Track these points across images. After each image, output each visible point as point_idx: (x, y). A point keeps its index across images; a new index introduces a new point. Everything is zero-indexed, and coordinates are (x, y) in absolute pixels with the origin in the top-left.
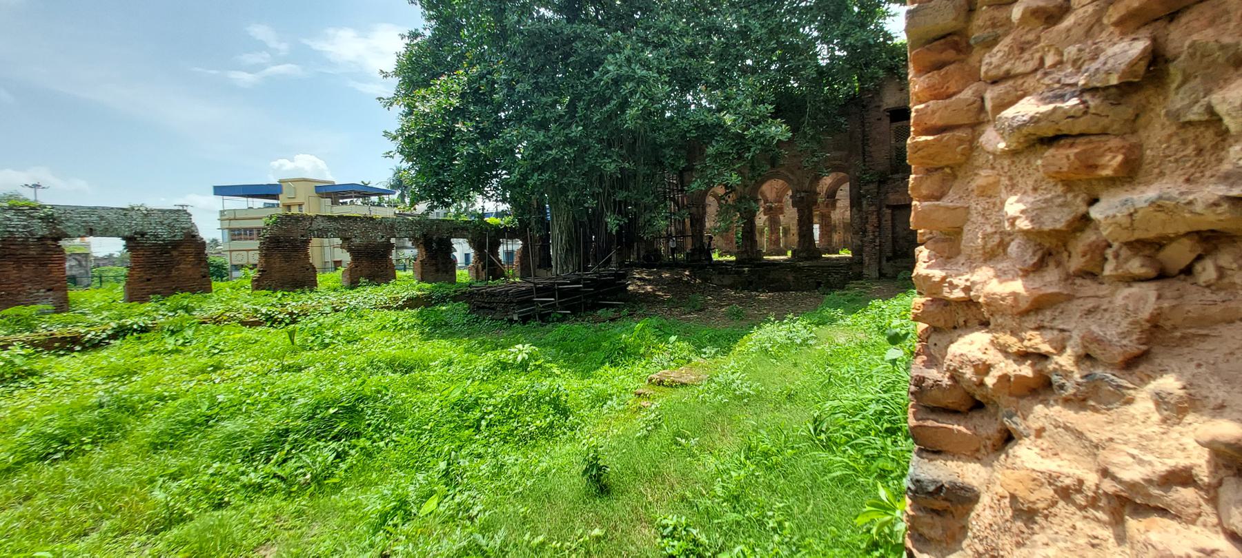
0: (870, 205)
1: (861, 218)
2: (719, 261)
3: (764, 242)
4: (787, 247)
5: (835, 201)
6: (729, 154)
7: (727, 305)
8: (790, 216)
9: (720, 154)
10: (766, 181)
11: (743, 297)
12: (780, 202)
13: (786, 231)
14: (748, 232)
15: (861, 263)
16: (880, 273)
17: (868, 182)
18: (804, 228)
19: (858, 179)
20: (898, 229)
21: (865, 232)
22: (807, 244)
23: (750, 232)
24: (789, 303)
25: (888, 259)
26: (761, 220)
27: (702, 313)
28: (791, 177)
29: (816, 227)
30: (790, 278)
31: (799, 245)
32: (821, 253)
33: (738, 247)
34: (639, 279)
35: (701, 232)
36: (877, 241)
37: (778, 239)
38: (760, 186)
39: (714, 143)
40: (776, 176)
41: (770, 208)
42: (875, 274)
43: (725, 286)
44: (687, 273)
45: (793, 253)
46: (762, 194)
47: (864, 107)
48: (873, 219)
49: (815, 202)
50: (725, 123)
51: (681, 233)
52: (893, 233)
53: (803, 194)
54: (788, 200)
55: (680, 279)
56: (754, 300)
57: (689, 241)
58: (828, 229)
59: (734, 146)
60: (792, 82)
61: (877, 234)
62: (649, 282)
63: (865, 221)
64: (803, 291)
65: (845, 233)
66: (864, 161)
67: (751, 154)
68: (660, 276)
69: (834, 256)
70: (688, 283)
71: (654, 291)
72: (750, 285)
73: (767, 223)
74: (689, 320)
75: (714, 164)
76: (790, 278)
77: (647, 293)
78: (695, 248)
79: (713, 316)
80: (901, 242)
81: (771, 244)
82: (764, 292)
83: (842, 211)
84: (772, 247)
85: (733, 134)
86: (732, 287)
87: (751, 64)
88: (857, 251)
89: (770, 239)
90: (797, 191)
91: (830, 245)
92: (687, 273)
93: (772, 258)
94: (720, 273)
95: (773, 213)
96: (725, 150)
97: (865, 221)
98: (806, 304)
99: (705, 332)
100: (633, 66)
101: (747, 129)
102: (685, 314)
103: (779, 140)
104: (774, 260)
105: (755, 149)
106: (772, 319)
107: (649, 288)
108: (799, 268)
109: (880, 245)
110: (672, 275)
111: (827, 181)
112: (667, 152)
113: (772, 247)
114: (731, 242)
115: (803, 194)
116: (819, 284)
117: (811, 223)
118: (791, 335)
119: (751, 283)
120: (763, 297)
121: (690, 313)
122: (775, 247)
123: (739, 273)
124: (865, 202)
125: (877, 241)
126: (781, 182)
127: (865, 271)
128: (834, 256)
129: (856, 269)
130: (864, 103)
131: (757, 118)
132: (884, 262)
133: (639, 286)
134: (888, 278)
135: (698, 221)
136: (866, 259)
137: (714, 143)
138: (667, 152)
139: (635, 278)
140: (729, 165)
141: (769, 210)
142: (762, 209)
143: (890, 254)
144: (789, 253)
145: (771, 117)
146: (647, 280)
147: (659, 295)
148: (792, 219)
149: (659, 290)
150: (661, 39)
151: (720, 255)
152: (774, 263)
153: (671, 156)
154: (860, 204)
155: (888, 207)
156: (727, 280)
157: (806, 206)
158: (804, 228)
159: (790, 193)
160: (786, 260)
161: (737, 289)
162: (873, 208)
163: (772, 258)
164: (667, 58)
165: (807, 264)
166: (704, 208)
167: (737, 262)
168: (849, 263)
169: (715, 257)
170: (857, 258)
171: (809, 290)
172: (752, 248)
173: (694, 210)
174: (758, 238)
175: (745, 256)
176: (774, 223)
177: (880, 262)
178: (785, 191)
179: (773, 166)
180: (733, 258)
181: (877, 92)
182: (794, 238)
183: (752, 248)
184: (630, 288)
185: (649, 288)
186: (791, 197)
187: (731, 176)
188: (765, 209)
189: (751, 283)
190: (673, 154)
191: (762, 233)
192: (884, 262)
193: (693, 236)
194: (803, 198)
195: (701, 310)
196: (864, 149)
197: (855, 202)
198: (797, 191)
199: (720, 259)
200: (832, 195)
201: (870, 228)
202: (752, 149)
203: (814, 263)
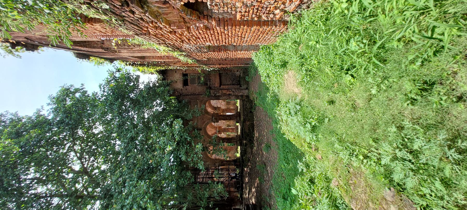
0: (219, 92)
1: (224, 96)
2: (240, 153)
3: (232, 134)
4: (235, 125)
5: (218, 107)
6: (187, 148)
7: (262, 151)
8: (222, 124)
9: (187, 153)
10: (207, 133)
11: (257, 143)
12: (216, 128)
13: (229, 126)
14: (228, 141)
15: (242, 96)
16: (246, 89)
17: (210, 93)
18: (228, 118)
19: (208, 96)
20: (229, 83)
21: (229, 95)
22: (234, 117)
23: (228, 140)
24: (260, 123)
25: (241, 86)
26: (223, 135)
27: (267, 164)
28: (206, 123)
29: (227, 114)
30: (248, 123)
31: (234, 120)
32: (238, 112)
33: (234, 145)
34: (249, 195)
35: (227, 161)
36: (233, 90)
37: (231, 129)
38: (209, 135)
39: (181, 156)
40: (205, 128)
41: (219, 131)
42: (247, 91)
43: (252, 152)
44: (246, 169)
45: (237, 122)
46: (213, 134)
47: (181, 95)
48: (224, 92)
49: (217, 114)
50: (171, 151)
51: (228, 170)
52: (230, 85)
53: (214, 118)
54: (215, 124)
55: (249, 173)
56: (258, 138)
57: (231, 167)
58: (228, 110)
59: (183, 146)
60: (168, 122)
61: (230, 90)
62: (250, 190)
63: (225, 95)
64: (254, 118)
65: (230, 105)
66: (201, 95)
67: (188, 138)
68: (247, 183)
69: (239, 107)
70: (250, 169)
71: (255, 187)
72: (251, 141)
73: (225, 133)
74: (272, 172)
75: (191, 156)
76: (248, 123)
77: (257, 191)
78: (234, 164)
79: (269, 158)
80: (234, 82)
81: (234, 132)
82: (254, 134)
83: (221, 104)
84: (235, 131)
85: (177, 146)
86: (252, 148)
87: (96, 131)
88: (237, 97)
89: (231, 132)
90: (212, 120)
91: (234, 109)
92: (246, 169)
93: (239, 131)
94: (246, 154)
95: (221, 130)
96: (184, 151)
97: (225, 95)
98: (260, 116)
99: (282, 166)
100: (126, 204)
101: (175, 139)
102: (268, 173)
103: (182, 124)
104: (240, 130)
105: (186, 135)
106: (279, 126)
107: (253, 190)
108: (244, 119)
109: (235, 89)
110: (247, 177)
111: (209, 110)
112: (181, 182)
113: (235, 131)
114: (232, 148)
115: (214, 118)
116: (251, 112)
117: (226, 115)
118: (293, 113)
119: (250, 140)
120: (257, 135)
121: (267, 171)
122: (235, 130)
123: (246, 145)
124: (218, 94)
125: (233, 90)
126: (208, 127)
127: (246, 94)
128: (239, 107)
129: (244, 98)
130: (179, 94)
131: (171, 134)
132: (242, 88)
133: (252, 195)
134: (248, 87)
135: (222, 162)
136: (240, 94)
137: (181, 156)
138: (181, 182)
139: (248, 197)
140: (192, 148)
141: (220, 132)
142: (219, 135)
143: (239, 86)
144: (238, 124)
145: (172, 128)
146: (249, 190)
147: (257, 185)
148: (224, 123)
149: (255, 184)
150: (121, 184)
151: (238, 152)
152: (242, 130)
153: (184, 180)
154: (219, 96)
155: (220, 86)
156: (249, 150)
157: (218, 117)
158: (228, 118)
159: (213, 124)
160: (240, 125)
161: (253, 146)
162: (220, 91)
163: (239, 131)
164: (131, 181)
165: (242, 117)
166: (216, 159)
167: (241, 146)
168: (243, 101)
169: (238, 155)
170: (240, 98)
171: (253, 116)
172: (234, 139)
173: (217, 164)
174: (230, 137)
175: (238, 142)
176: (225, 130)
177: (241, 89)
178: (212, 126)
179: (201, 130)
180: (239, 147)
181: (175, 90)
182: (231, 122)
183: (234, 139)
184: (254, 202)
185: (253, 190)
186: (214, 123)
187: (197, 148)
188: (219, 134)
189: (250, 140)
190: (182, 179)
191: (229, 135)
192: (242, 88)
193: (229, 165)
194: (215, 118)
195: (265, 165)
196: (197, 95)
197: (217, 98)
198: (212, 120)
199: (239, 153)
200: (215, 108)
201: (228, 93)
202: (186, 137)
203: (242, 114)
